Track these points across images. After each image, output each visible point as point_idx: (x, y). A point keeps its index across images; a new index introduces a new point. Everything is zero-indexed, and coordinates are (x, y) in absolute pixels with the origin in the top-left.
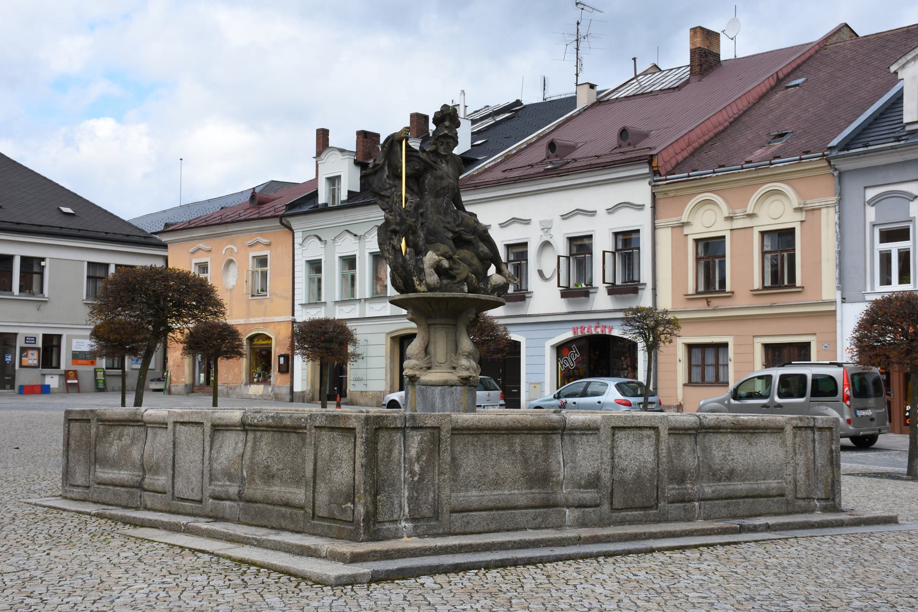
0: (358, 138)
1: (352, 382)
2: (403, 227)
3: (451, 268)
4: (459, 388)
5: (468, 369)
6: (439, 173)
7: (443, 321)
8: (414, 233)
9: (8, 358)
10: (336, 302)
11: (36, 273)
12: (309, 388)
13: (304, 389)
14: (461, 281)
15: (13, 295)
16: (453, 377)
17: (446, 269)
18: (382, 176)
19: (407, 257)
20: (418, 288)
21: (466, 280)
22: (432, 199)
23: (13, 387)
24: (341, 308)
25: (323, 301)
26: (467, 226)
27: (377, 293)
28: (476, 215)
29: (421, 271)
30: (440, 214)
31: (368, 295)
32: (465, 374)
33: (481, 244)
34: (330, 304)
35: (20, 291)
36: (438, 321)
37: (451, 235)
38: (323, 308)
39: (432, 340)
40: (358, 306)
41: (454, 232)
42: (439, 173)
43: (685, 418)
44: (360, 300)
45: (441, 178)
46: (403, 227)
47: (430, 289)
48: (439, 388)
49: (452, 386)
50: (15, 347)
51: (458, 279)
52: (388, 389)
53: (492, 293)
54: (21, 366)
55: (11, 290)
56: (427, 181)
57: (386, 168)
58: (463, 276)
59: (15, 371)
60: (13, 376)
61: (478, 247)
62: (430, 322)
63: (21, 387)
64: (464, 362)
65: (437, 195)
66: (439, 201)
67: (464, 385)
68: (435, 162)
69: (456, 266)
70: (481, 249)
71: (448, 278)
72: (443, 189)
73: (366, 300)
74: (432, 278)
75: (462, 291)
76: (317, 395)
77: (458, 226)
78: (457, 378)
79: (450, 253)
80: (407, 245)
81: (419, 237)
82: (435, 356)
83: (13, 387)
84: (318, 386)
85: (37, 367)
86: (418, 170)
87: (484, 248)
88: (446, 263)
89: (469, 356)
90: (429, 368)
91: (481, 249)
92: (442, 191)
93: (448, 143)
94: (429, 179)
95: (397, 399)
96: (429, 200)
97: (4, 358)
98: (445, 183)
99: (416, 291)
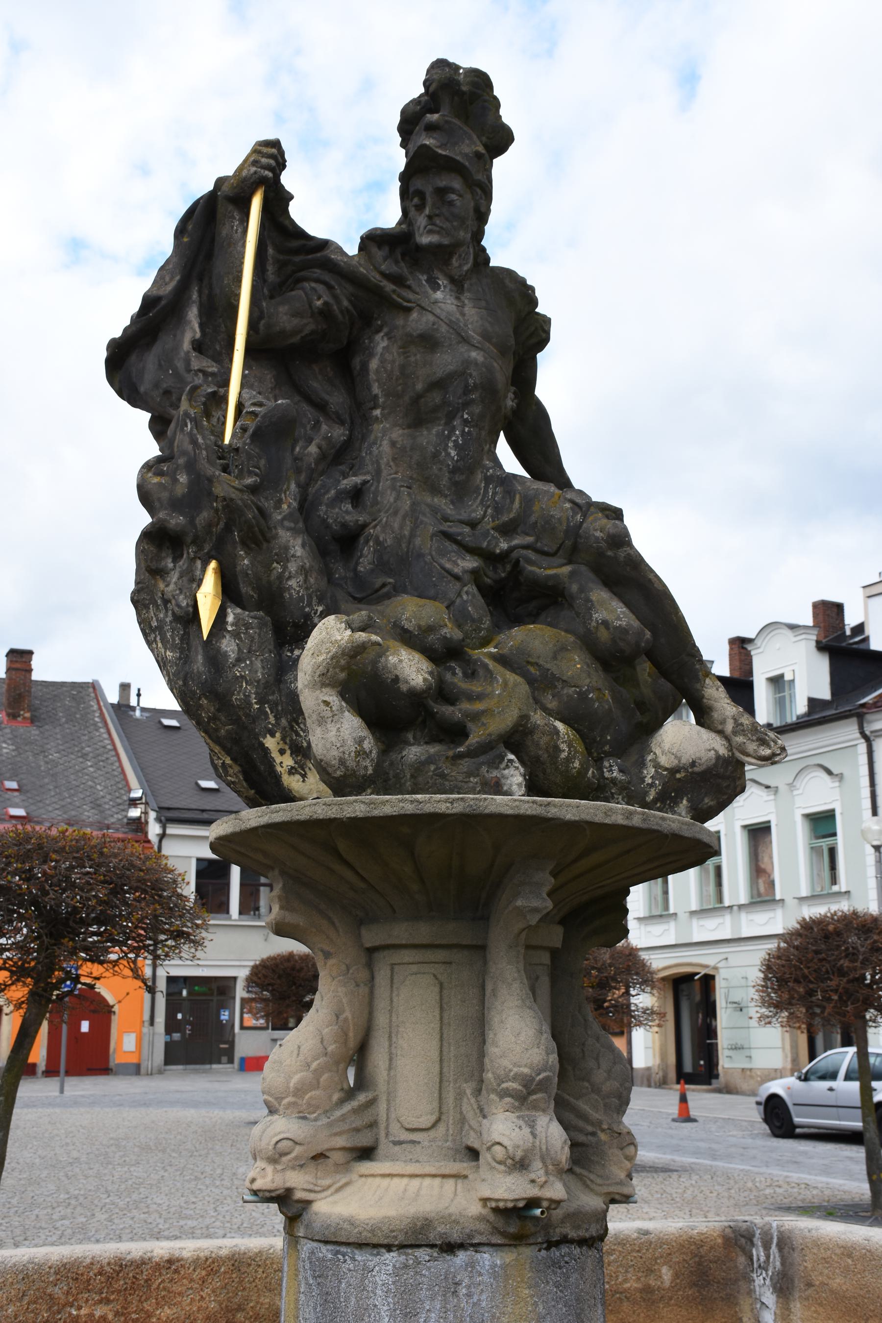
0: (731, 649)
1: (727, 1053)
2: (204, 516)
3: (442, 692)
4: (486, 1259)
5: (520, 1165)
6: (417, 322)
7: (424, 932)
8: (258, 538)
9: (225, 1016)
10: (693, 913)
11: (264, 885)
12: (658, 1061)
13: (650, 1064)
14: (485, 748)
15: (230, 919)
16: (460, 1200)
17: (416, 697)
18: (177, 347)
19: (229, 646)
20: (293, 783)
21: (517, 739)
22: (397, 434)
23: (231, 1061)
24: (702, 922)
25: (672, 911)
26: (546, 527)
27: (759, 895)
28: (617, 514)
29: (293, 711)
30: (435, 490)
31: (743, 898)
32: (509, 1188)
33: (600, 595)
34: (683, 917)
35: (241, 913)
36: (400, 932)
37: (469, 563)
38: (672, 924)
39: (381, 1019)
40: (727, 919)
41: (490, 558)
42: (417, 322)
43: (405, 270)
44: (730, 907)
45: (428, 341)
46: (204, 516)
47: (342, 784)
48: (391, 1258)
49: (450, 1248)
50: (234, 998)
51: (473, 739)
52: (789, 1066)
53: (667, 799)
54: (242, 1027)
55: (228, 912)
56: (374, 364)
57: (193, 314)
58: (501, 722)
59: (234, 1035)
60: (232, 1044)
61: (589, 606)
62: (372, 937)
63: (243, 1060)
64: (504, 1128)
65: (418, 417)
66: (428, 437)
67: (517, 1240)
68: (398, 280)
69: (476, 687)
70: (598, 616)
71: (433, 740)
72: (439, 384)
73: (740, 907)
74: (338, 732)
75: (497, 788)
76: (672, 1074)
77: (507, 530)
78: (475, 1209)
79: (450, 631)
80: (229, 591)
81: (284, 557)
82: (391, 1096)
83: (231, 1061)
84: (672, 1059)
85: (266, 1028)
86: (325, 313)
87: (611, 611)
88: (412, 669)
89: (525, 1095)
90: (366, 1153)
91: (598, 616)
92: (436, 397)
93: (441, 192)
94: (381, 354)
95: (781, 1092)
96: (386, 437)
97: (219, 1015)
98: (444, 362)
99: (288, 797)
